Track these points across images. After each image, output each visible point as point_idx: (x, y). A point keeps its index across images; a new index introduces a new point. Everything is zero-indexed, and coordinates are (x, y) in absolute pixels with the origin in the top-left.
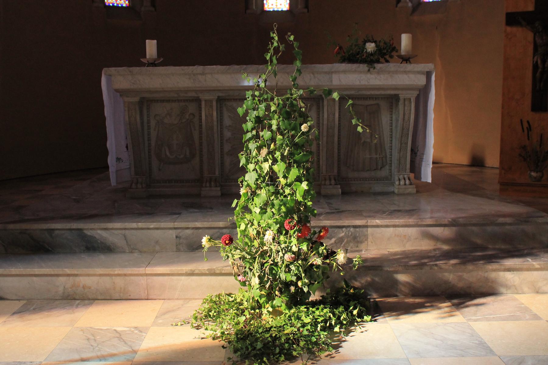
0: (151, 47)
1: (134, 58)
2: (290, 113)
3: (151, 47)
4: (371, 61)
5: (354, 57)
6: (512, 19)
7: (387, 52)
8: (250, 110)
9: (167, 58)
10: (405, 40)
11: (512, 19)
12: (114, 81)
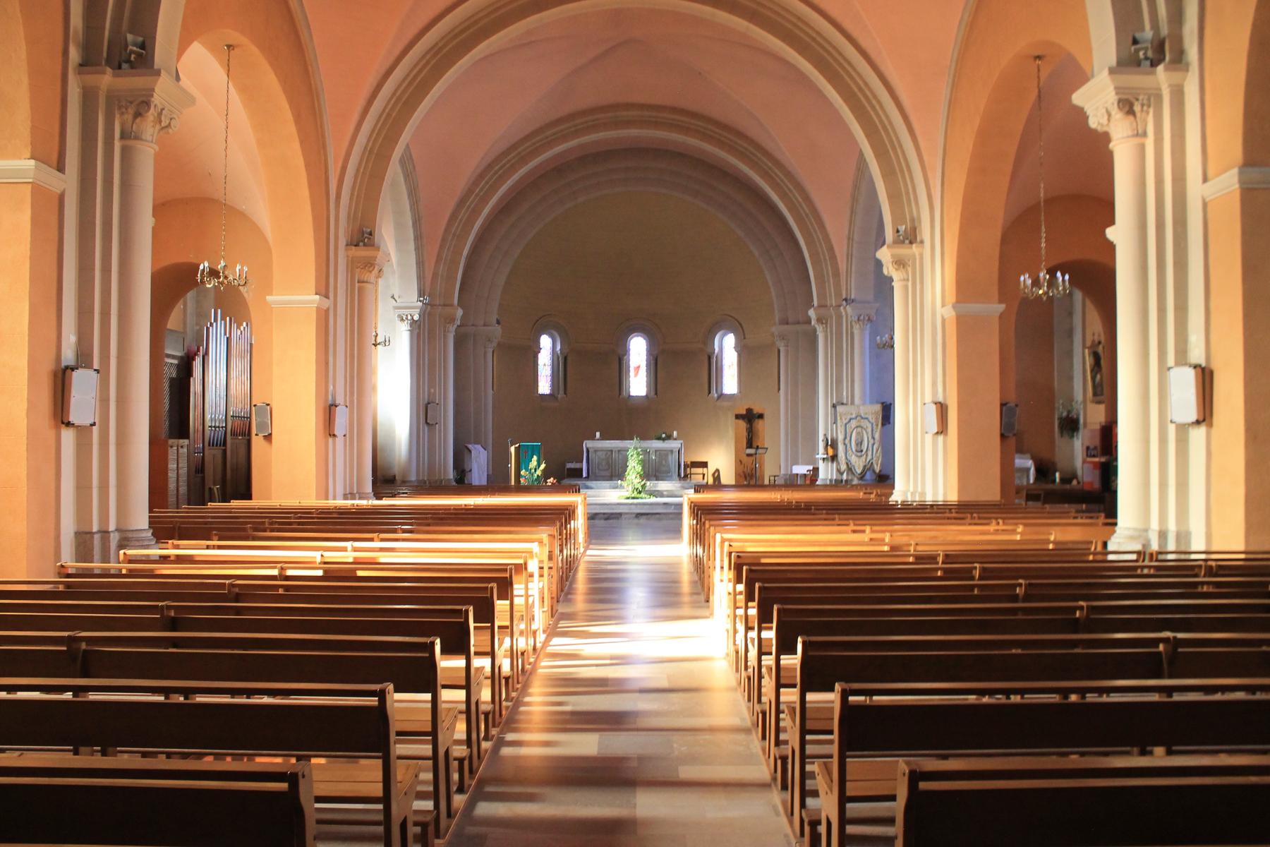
0: (598, 434)
1: (593, 438)
2: (638, 454)
3: (598, 434)
4: (664, 440)
5: (659, 438)
6: (738, 417)
7: (669, 437)
8: (630, 453)
9: (603, 438)
11: (738, 417)
12: (588, 444)
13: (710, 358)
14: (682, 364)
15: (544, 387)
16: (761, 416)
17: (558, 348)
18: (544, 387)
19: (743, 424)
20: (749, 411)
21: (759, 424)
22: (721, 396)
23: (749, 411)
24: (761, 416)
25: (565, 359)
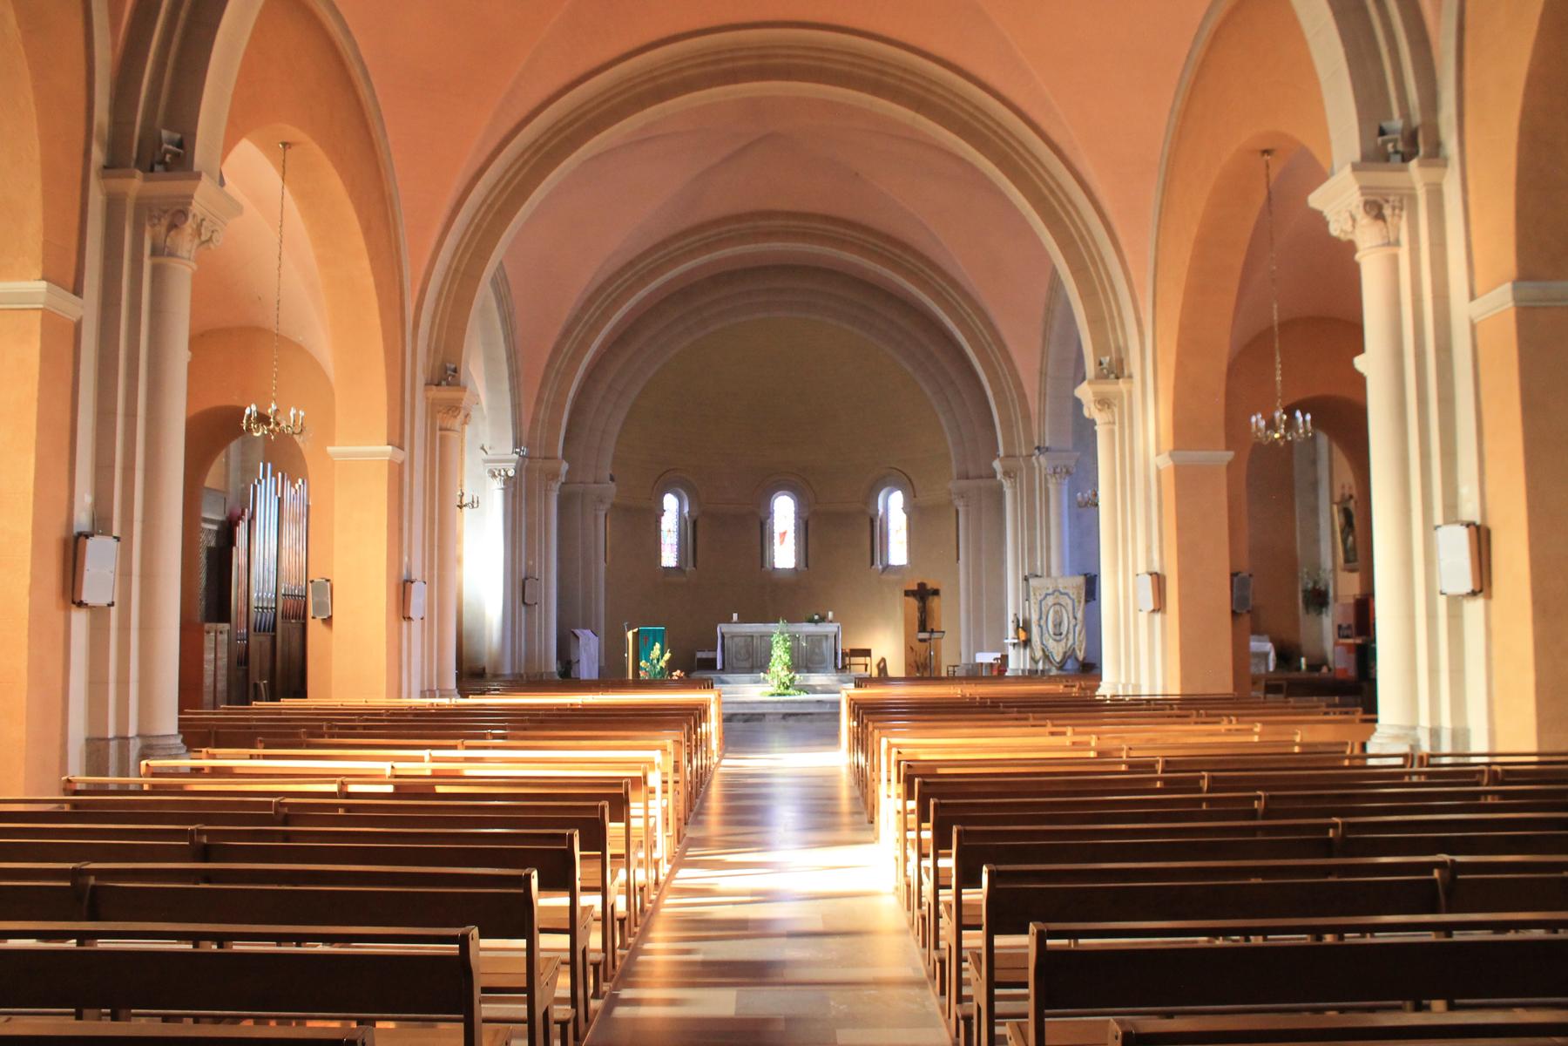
0: (735, 616)
1: (729, 620)
2: (785, 640)
3: (735, 616)
4: (816, 622)
5: (811, 621)
6: (907, 593)
7: (823, 619)
8: (775, 639)
9: (742, 620)
10: (830, 614)
11: (907, 593)
12: (722, 628)
13: (872, 522)
14: (839, 529)
15: (669, 558)
16: (936, 592)
17: (686, 510)
18: (669, 558)
19: (913, 603)
20: (922, 586)
21: (934, 603)
22: (887, 567)
23: (922, 586)
24: (936, 592)
25: (695, 523)
